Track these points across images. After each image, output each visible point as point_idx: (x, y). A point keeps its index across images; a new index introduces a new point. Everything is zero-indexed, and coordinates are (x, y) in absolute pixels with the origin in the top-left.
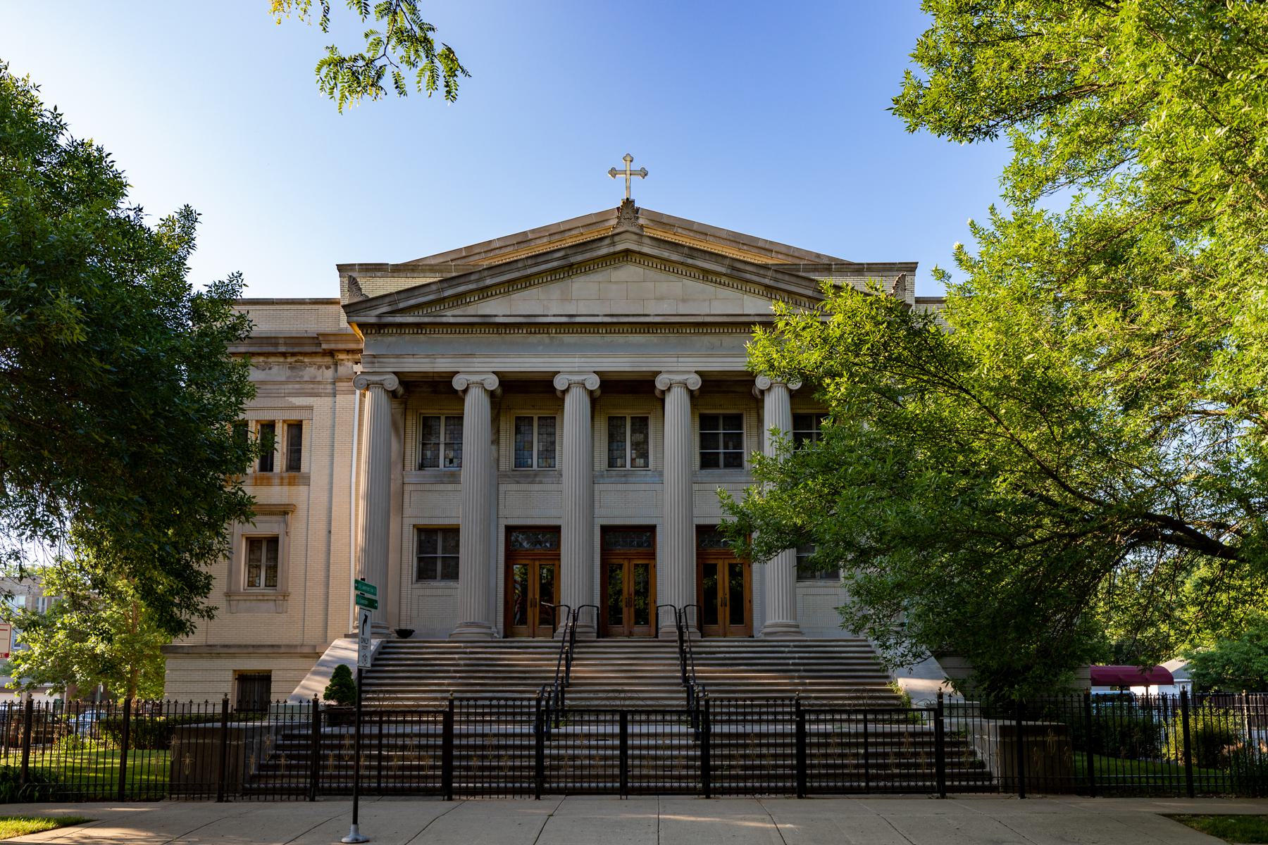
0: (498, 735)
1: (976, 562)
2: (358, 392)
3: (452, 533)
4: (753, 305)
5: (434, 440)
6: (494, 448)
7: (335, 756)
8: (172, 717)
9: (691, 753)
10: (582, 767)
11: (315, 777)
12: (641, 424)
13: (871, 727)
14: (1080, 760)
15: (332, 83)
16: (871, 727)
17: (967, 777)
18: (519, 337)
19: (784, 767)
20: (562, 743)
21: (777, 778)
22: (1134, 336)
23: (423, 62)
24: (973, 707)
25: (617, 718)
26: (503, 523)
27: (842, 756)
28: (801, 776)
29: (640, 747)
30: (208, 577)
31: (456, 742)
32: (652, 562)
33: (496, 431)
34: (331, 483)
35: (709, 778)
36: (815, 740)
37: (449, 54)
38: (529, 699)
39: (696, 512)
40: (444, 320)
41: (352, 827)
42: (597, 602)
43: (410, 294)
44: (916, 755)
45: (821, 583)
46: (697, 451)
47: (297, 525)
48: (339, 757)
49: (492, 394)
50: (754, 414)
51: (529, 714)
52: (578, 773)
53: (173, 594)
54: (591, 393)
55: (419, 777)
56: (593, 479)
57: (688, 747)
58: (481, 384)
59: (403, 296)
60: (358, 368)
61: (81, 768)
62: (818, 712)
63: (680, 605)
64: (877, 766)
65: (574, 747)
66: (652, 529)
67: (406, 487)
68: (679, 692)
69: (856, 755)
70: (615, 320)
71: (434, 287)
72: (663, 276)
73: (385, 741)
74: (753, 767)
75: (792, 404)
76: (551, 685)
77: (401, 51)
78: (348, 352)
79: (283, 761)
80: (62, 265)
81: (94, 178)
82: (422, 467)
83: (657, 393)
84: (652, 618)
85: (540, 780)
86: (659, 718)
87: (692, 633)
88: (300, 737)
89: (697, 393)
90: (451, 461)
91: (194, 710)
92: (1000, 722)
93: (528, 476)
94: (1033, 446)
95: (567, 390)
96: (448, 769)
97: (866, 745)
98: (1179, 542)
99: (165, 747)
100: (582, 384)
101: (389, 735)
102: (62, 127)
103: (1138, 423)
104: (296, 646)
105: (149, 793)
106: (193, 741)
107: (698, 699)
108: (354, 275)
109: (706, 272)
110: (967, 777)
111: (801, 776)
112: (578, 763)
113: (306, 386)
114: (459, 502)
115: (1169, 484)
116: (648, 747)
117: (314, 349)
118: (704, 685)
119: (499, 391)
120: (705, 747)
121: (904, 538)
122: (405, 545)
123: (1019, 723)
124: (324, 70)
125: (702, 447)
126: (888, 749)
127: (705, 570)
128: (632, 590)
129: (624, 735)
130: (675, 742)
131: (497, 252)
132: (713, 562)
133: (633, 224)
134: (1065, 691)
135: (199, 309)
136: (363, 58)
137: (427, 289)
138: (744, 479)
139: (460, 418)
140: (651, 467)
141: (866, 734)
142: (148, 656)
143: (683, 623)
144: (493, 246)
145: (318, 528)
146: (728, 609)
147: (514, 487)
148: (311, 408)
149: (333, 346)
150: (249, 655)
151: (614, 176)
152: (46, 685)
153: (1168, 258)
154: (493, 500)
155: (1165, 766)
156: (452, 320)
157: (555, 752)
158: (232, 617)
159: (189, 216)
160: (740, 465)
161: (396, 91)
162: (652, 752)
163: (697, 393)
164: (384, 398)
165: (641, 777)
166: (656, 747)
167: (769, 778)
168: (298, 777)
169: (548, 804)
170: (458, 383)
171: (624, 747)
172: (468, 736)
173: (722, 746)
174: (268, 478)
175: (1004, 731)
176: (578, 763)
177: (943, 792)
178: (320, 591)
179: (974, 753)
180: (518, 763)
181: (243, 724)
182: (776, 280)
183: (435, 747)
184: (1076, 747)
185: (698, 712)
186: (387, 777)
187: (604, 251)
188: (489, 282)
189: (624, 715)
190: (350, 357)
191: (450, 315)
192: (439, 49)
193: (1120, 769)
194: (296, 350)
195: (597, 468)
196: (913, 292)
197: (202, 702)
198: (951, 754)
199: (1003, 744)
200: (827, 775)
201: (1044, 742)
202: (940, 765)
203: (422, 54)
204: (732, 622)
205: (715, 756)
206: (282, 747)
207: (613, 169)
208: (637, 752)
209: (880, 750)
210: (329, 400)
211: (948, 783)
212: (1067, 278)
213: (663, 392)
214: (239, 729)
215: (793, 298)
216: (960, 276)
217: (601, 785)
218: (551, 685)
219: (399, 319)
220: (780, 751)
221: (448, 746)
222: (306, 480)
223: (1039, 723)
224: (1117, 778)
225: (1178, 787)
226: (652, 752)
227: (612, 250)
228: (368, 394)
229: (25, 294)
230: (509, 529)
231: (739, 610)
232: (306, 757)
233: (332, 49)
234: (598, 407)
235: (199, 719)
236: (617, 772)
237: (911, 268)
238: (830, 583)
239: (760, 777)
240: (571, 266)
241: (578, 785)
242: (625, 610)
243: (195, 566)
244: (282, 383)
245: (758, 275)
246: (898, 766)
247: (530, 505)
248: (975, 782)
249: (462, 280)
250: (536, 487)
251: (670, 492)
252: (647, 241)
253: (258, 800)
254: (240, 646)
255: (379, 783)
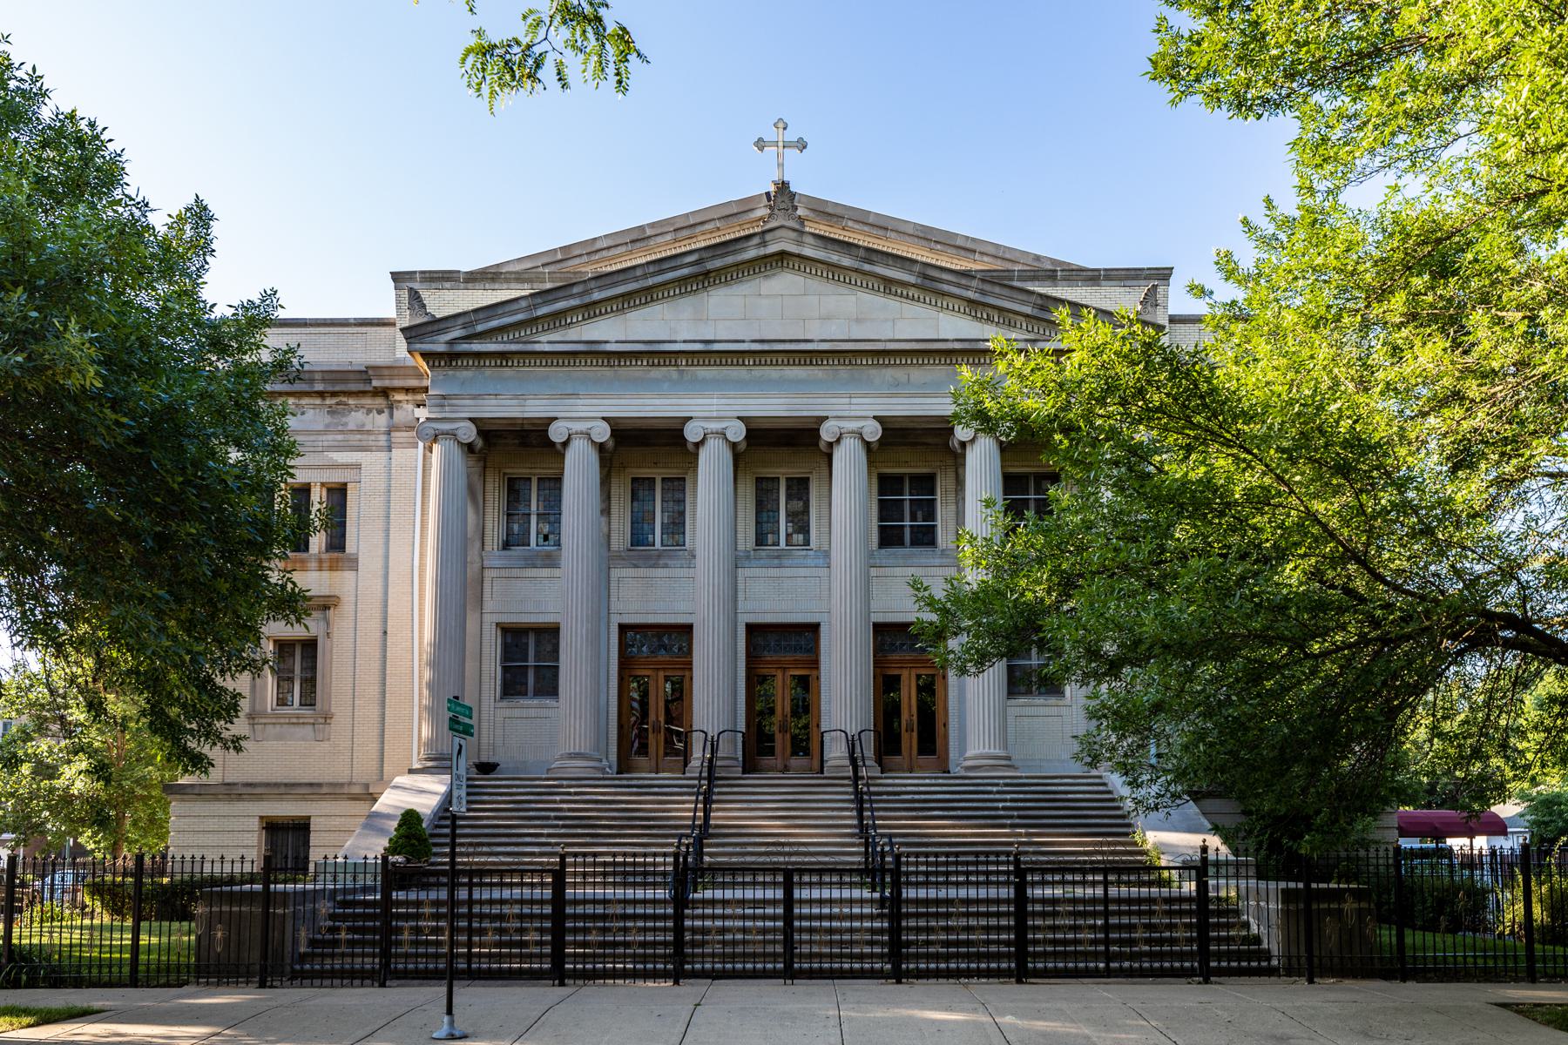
0: (625, 902)
1: (1255, 674)
2: (421, 445)
3: (549, 634)
4: (953, 326)
5: (522, 509)
6: (604, 519)
7: (411, 928)
8: (178, 877)
9: (877, 925)
10: (734, 943)
11: (386, 955)
12: (799, 488)
13: (1113, 891)
14: (1387, 935)
15: (480, 75)
16: (1113, 891)
17: (1239, 956)
18: (636, 371)
19: (998, 942)
20: (709, 911)
21: (989, 957)
22: (1467, 372)
23: (592, 42)
24: (1247, 864)
25: (780, 879)
26: (616, 620)
27: (1075, 928)
28: (1021, 955)
29: (811, 917)
30: (236, 696)
31: (569, 910)
32: (814, 673)
33: (606, 497)
34: (386, 567)
35: (903, 952)
36: (1038, 908)
37: (623, 35)
38: (665, 855)
39: (874, 606)
40: (537, 347)
41: (446, 1019)
42: (742, 726)
43: (490, 313)
44: (1171, 927)
45: (1040, 701)
46: (875, 523)
47: (342, 622)
48: (417, 930)
49: (601, 447)
50: (951, 475)
51: (664, 874)
52: (728, 950)
53: (186, 715)
54: (734, 446)
55: (521, 955)
56: (737, 562)
57: (872, 917)
58: (587, 435)
59: (481, 315)
60: (422, 414)
61: (81, 945)
62: (1044, 871)
63: (853, 730)
64: (1121, 942)
65: (724, 917)
66: (814, 628)
67: (488, 574)
68: (853, 845)
69: (1093, 928)
70: (766, 347)
71: (524, 304)
72: (830, 287)
73: (476, 909)
74: (958, 943)
75: (1003, 460)
76: (687, 836)
77: (565, 33)
78: (407, 390)
79: (343, 935)
80: (63, 287)
81: (84, 165)
82: (506, 545)
83: (822, 445)
84: (815, 746)
85: (678, 959)
86: (835, 879)
87: (869, 770)
88: (366, 904)
89: (875, 447)
90: (546, 538)
91: (207, 869)
92: (1282, 885)
93: (649, 558)
94: (1334, 523)
95: (702, 442)
96: (558, 944)
97: (1106, 914)
98: (1524, 647)
99: (186, 916)
100: (722, 434)
101: (481, 902)
102: (44, 95)
103: (1470, 491)
104: (342, 785)
105: (169, 975)
106: (235, 909)
107: (883, 854)
108: (416, 286)
109: (888, 282)
110: (1239, 956)
111: (1021, 955)
112: (729, 937)
113: (351, 437)
114: (557, 593)
115: (1509, 570)
116: (821, 917)
117: (361, 387)
118: (890, 836)
119: (611, 444)
120: (896, 917)
121: (1166, 647)
122: (486, 650)
123: (1307, 886)
124: (471, 59)
125: (881, 519)
126: (1135, 920)
127: (886, 684)
128: (788, 709)
129: (789, 902)
130: (856, 910)
131: (604, 253)
132: (896, 672)
133: (790, 217)
134: (1364, 844)
135: (218, 338)
136: (518, 43)
137: (515, 306)
138: (937, 561)
139: (558, 480)
140: (813, 545)
141: (1106, 900)
142: (142, 798)
143: (858, 754)
144: (599, 245)
145: (371, 627)
146: (915, 734)
147: (631, 572)
148: (358, 466)
149: (387, 383)
150: (281, 797)
151: (761, 149)
152: (5, 836)
153: (1518, 268)
154: (603, 589)
155: (1500, 943)
156: (547, 348)
157: (698, 923)
158: (267, 749)
159: (200, 215)
160: (932, 542)
161: (559, 85)
162: (826, 924)
163: (875, 447)
164: (457, 452)
165: (811, 956)
166: (831, 917)
167: (979, 957)
168: (363, 955)
169: (690, 990)
170: (556, 433)
171: (788, 917)
172: (585, 902)
173: (917, 916)
174: (303, 561)
175: (1287, 895)
176: (729, 937)
177: (1206, 975)
178: (374, 711)
179: (1247, 925)
180: (650, 938)
181: (290, 886)
182: (983, 292)
183: (542, 917)
184: (1382, 919)
185: (883, 871)
186: (480, 955)
187: (752, 254)
188: (596, 296)
189: (788, 874)
190: (409, 397)
191: (546, 341)
192: (611, 28)
193: (1440, 945)
194: (338, 388)
195: (741, 547)
196: (1166, 307)
197: (217, 858)
198: (1218, 926)
199: (1286, 913)
200: (1055, 953)
201: (1340, 911)
202: (1203, 940)
203: (590, 34)
204: (921, 752)
205: (908, 929)
206: (344, 917)
207: (761, 139)
208: (805, 924)
209: (1125, 920)
210: (383, 455)
211: (1213, 964)
212: (1383, 294)
213: (830, 445)
214: (285, 893)
215: (1006, 317)
216: (1228, 292)
217: (759, 966)
218: (687, 836)
219: (476, 347)
220: (993, 922)
221: (558, 916)
222: (353, 564)
223: (1333, 885)
224: (1435, 958)
225: (1516, 970)
226: (826, 924)
227: (762, 252)
228: (435, 447)
229: (23, 326)
230: (623, 628)
231: (931, 737)
232: (374, 930)
233: (479, 33)
234: (741, 465)
235: (231, 880)
236: (779, 949)
237: (1164, 274)
238: (1052, 700)
239: (968, 957)
240: (707, 274)
241: (729, 966)
242: (778, 737)
243: (219, 680)
244: (318, 433)
245: (958, 285)
246: (1148, 941)
247: (648, 597)
248: (1248, 963)
249: (561, 294)
250: (660, 572)
251: (839, 580)
252: (810, 240)
253: (312, 986)
254: (267, 785)
255: (469, 963)
